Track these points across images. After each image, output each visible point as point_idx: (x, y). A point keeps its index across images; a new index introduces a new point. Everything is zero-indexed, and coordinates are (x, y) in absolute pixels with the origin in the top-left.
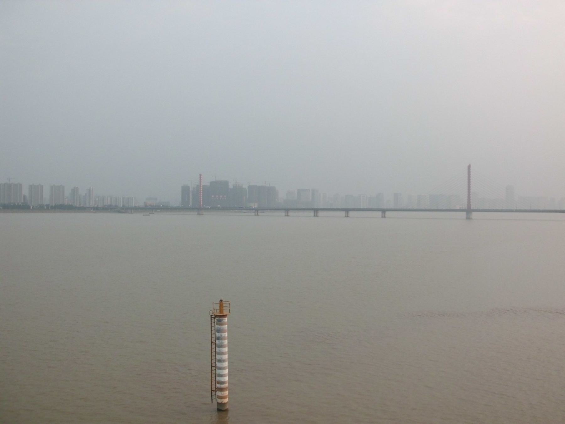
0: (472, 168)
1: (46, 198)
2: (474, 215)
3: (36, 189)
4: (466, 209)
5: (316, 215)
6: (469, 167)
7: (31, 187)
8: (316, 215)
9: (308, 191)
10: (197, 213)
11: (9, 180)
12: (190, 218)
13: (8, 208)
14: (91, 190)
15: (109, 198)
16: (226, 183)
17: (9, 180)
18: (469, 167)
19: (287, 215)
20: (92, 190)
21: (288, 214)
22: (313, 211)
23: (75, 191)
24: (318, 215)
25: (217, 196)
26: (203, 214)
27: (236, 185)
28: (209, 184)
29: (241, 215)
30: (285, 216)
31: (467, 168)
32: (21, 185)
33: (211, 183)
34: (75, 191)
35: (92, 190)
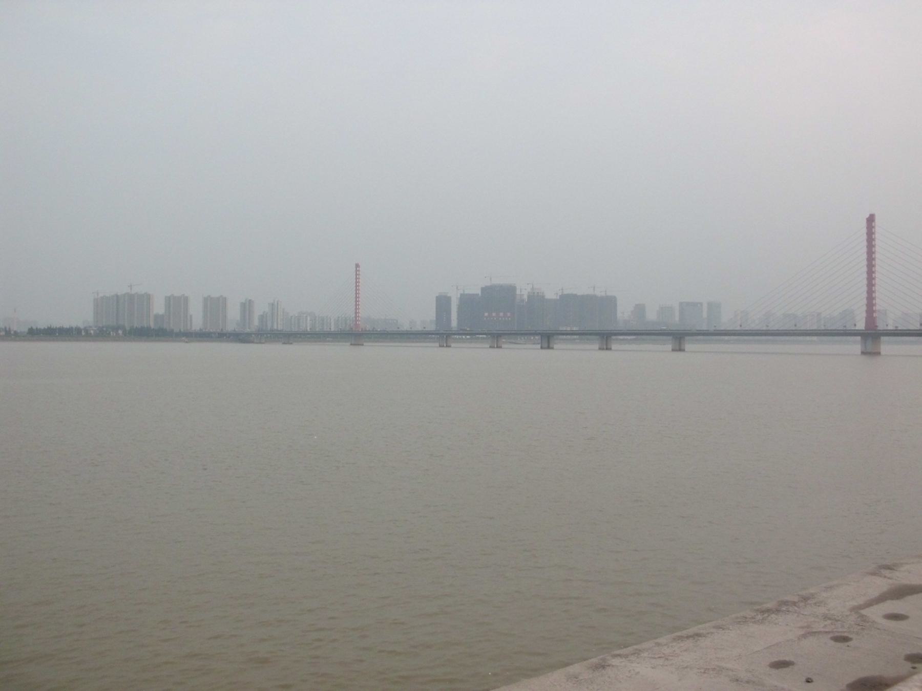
0: (878, 222)
1: (197, 322)
2: (887, 347)
3: (177, 304)
4: (864, 329)
5: (871, 353)
6: (871, 220)
7: (168, 300)
8: (871, 353)
9: (699, 305)
10: (437, 344)
11: (131, 289)
12: (429, 351)
13: (9, 335)
14: (276, 303)
15: (309, 319)
16: (511, 289)
17: (131, 289)
18: (871, 220)
19: (678, 348)
20: (278, 304)
21: (607, 345)
22: (540, 336)
23: (247, 307)
24: (551, 346)
25: (501, 314)
26: (363, 345)
27: (534, 293)
28: (479, 292)
29: (641, 351)
30: (673, 350)
31: (864, 224)
32: (186, 299)
33: (483, 289)
34: (247, 307)
35: (278, 304)
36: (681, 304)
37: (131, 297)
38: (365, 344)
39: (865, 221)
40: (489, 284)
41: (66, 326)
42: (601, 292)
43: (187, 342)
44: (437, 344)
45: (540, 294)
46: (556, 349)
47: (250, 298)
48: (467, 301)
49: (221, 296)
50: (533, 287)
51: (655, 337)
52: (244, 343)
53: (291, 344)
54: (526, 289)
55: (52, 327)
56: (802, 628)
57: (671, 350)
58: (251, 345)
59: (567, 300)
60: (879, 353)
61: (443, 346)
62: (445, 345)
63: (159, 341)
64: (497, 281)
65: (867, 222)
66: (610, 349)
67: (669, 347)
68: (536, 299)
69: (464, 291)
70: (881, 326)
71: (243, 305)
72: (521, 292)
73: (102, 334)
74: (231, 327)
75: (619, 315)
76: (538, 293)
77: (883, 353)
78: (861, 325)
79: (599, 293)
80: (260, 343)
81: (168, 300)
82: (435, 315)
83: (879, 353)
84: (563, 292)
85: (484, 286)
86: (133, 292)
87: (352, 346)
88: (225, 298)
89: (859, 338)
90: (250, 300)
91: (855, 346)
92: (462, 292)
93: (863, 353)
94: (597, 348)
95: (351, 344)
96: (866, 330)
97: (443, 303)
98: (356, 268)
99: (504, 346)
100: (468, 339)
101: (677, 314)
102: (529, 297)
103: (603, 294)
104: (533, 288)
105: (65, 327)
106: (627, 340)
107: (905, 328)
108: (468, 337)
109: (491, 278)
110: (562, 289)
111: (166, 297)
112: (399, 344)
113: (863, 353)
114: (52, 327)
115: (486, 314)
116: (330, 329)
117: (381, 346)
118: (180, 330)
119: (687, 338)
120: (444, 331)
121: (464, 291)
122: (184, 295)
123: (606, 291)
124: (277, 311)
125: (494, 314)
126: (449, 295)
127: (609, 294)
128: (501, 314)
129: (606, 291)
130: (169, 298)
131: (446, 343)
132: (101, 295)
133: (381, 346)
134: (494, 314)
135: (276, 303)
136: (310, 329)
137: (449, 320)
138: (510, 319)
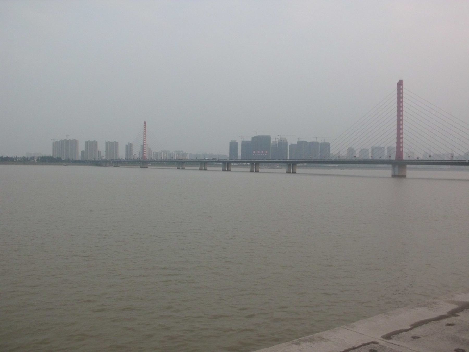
0: (405, 86)
1: (122, 154)
6: (400, 84)
7: (87, 143)
16: (268, 139)
18: (400, 84)
23: (129, 147)
24: (229, 169)
26: (147, 168)
30: (287, 172)
33: (253, 138)
37: (67, 142)
38: (120, 167)
39: (396, 85)
40: (256, 135)
41: (5, 156)
42: (322, 140)
43: (65, 165)
44: (176, 168)
45: (285, 141)
46: (233, 171)
47: (130, 143)
48: (245, 145)
49: (115, 141)
50: (281, 137)
51: (422, 166)
52: (98, 166)
53: (119, 167)
54: (278, 139)
56: (322, 339)
58: (99, 167)
59: (301, 144)
60: (404, 176)
61: (180, 169)
63: (50, 164)
64: (261, 134)
65: (397, 86)
66: (295, 173)
68: (282, 143)
69: (244, 139)
70: (405, 157)
71: (127, 146)
72: (275, 140)
74: (79, 157)
75: (331, 152)
76: (284, 141)
77: (408, 176)
78: (393, 157)
79: (320, 141)
80: (106, 166)
81: (87, 143)
83: (404, 176)
84: (299, 140)
85: (253, 137)
86: (68, 139)
87: (141, 168)
88: (117, 143)
89: (391, 165)
90: (131, 144)
91: (388, 172)
92: (243, 140)
93: (393, 176)
95: (141, 167)
96: (396, 160)
97: (233, 146)
98: (144, 123)
99: (233, 169)
101: (386, 152)
102: (279, 142)
103: (323, 141)
104: (281, 138)
105: (4, 157)
106: (329, 167)
107: (442, 159)
108: (248, 163)
109: (257, 132)
110: (299, 139)
113: (393, 176)
116: (161, 158)
120: (279, 160)
121: (244, 139)
122: (89, 141)
123: (324, 140)
125: (262, 152)
126: (236, 141)
127: (326, 141)
129: (324, 140)
132: (55, 141)
134: (258, 152)
136: (142, 158)
138: (267, 154)
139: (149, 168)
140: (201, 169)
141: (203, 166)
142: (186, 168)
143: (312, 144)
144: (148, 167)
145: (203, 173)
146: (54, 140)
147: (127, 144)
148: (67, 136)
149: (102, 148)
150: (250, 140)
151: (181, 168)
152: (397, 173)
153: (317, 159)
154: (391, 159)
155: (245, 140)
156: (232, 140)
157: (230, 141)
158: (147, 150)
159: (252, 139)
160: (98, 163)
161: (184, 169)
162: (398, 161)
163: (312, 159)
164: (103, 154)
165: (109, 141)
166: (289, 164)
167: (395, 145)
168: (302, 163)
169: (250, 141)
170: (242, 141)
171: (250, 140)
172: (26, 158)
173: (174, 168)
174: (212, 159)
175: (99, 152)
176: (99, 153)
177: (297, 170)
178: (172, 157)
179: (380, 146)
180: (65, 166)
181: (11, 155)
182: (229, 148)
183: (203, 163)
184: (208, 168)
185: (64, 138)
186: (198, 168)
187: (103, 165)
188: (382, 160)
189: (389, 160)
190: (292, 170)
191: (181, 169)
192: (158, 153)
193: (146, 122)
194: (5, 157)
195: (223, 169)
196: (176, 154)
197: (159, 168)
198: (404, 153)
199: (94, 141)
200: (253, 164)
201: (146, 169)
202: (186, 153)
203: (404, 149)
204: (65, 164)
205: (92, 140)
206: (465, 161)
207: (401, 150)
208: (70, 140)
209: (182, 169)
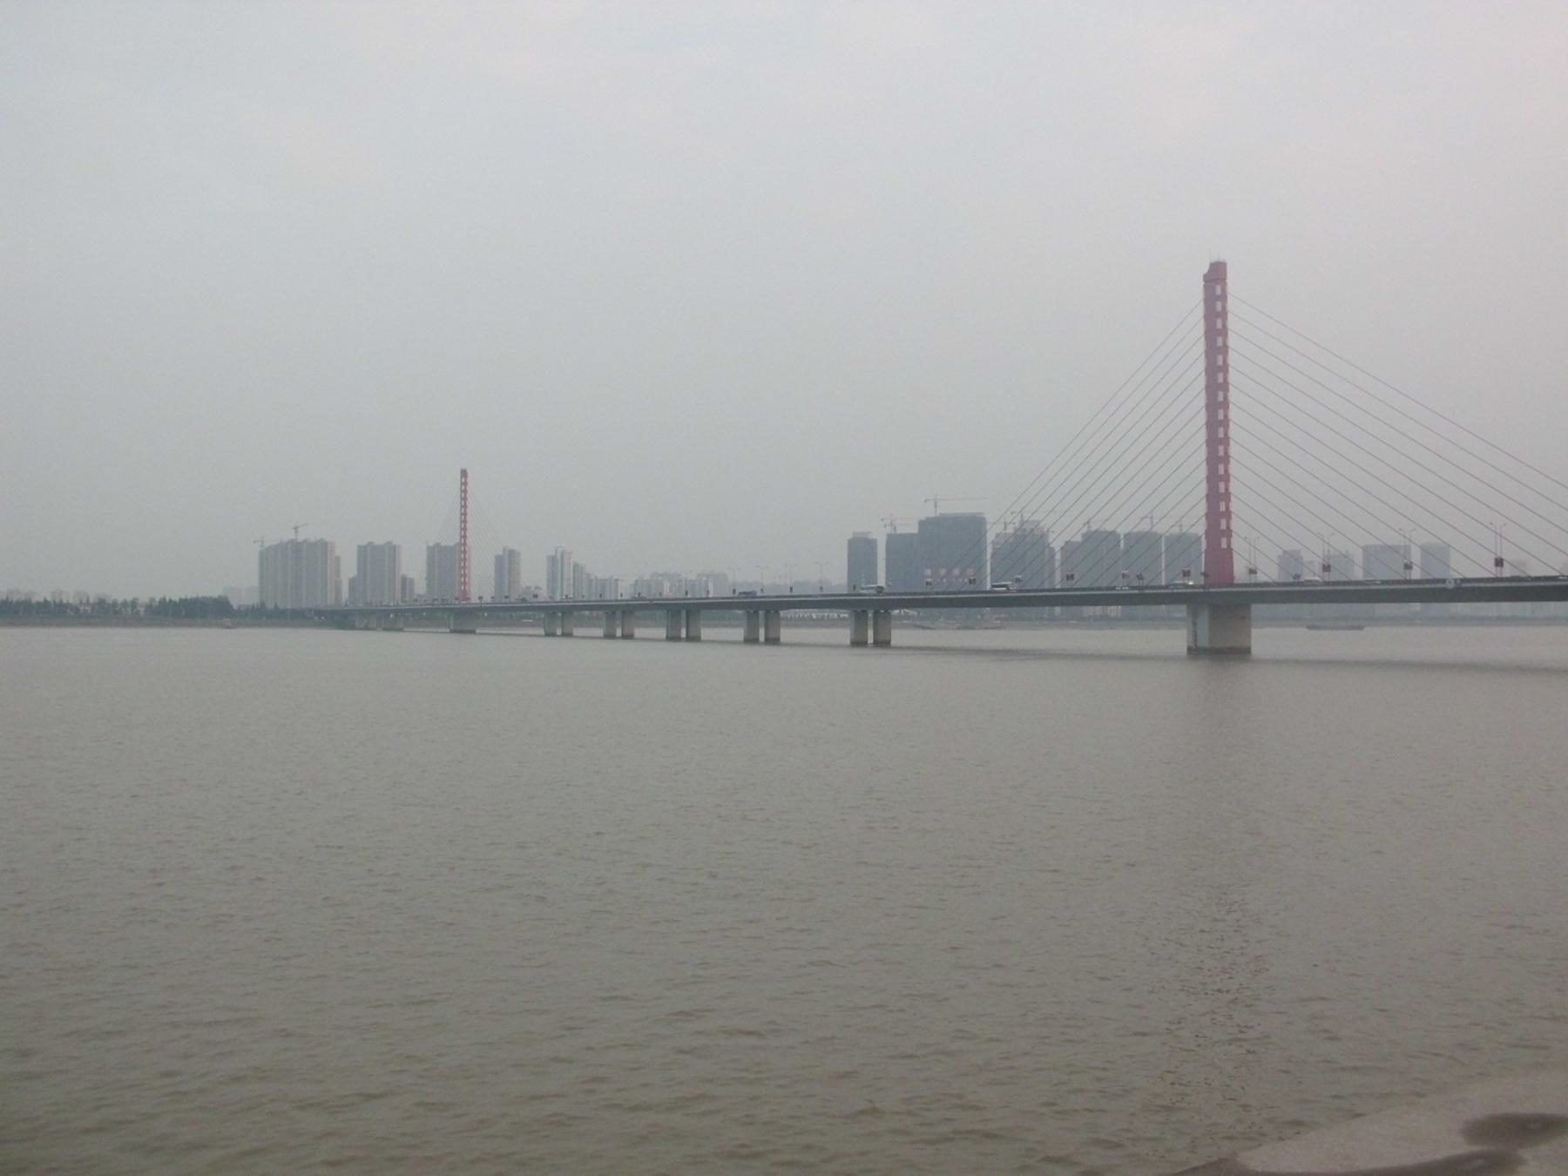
1: (481, 586)
6: (1216, 276)
7: (363, 552)
10: (739, 633)
11: (296, 532)
14: (559, 557)
17: (296, 532)
18: (1216, 276)
20: (562, 558)
23: (507, 563)
26: (473, 632)
34: (507, 563)
35: (562, 558)
36: (1365, 549)
38: (405, 630)
40: (932, 515)
44: (542, 632)
47: (512, 548)
48: (897, 544)
51: (1334, 606)
52: (343, 629)
53: (401, 630)
55: (10, 600)
57: (848, 642)
59: (1097, 541)
61: (554, 635)
62: (762, 638)
67: (844, 635)
71: (499, 560)
72: (1005, 528)
73: (261, 616)
77: (1257, 649)
80: (367, 628)
81: (363, 552)
82: (846, 575)
83: (1241, 653)
84: (1089, 527)
85: (923, 519)
86: (301, 538)
87: (453, 635)
88: (395, 547)
93: (1194, 652)
94: (664, 636)
95: (453, 632)
97: (860, 549)
100: (844, 618)
111: (359, 547)
112: (434, 630)
114: (10, 600)
115: (929, 572)
117: (531, 636)
118: (276, 606)
119: (1258, 609)
122: (370, 543)
124: (562, 567)
128: (956, 572)
130: (365, 547)
131: (563, 627)
133: (531, 636)
135: (559, 557)
137: (873, 576)
139: (480, 634)
140: (610, 636)
141: (684, 622)
142: (638, 632)
143: (1136, 539)
144: (477, 631)
145: (683, 652)
146: (263, 542)
147: (501, 553)
148: (296, 528)
149: (413, 567)
150: (914, 529)
151: (559, 632)
152: (1204, 642)
153: (1041, 588)
154: (1332, 579)
155: (899, 532)
156: (854, 533)
157: (850, 536)
158: (569, 573)
159: (920, 529)
160: (340, 619)
161: (570, 635)
162: (1202, 590)
163: (936, 590)
164: (420, 588)
165: (438, 545)
166: (859, 610)
167: (1200, 529)
168: (1421, 600)
169: (911, 535)
170: (889, 536)
171: (914, 529)
172: (109, 604)
173: (444, 630)
174: (737, 594)
175: (408, 582)
176: (406, 583)
177: (893, 632)
178: (507, 594)
179: (1190, 531)
180: (229, 630)
181: (119, 592)
182: (846, 562)
183: (761, 613)
184: (638, 632)
185: (288, 535)
186: (599, 632)
187: (357, 624)
188: (1147, 587)
189: (1327, 583)
190: (875, 634)
191: (557, 636)
192: (606, 580)
193: (468, 471)
194: (38, 603)
195: (667, 632)
196: (669, 584)
197: (495, 632)
198: (1236, 558)
199: (389, 543)
200: (864, 612)
201: (470, 638)
202: (616, 577)
203: (1236, 543)
204: (230, 624)
205: (379, 541)
206: (1444, 581)
207: (1224, 546)
208: (305, 541)
209: (564, 635)
